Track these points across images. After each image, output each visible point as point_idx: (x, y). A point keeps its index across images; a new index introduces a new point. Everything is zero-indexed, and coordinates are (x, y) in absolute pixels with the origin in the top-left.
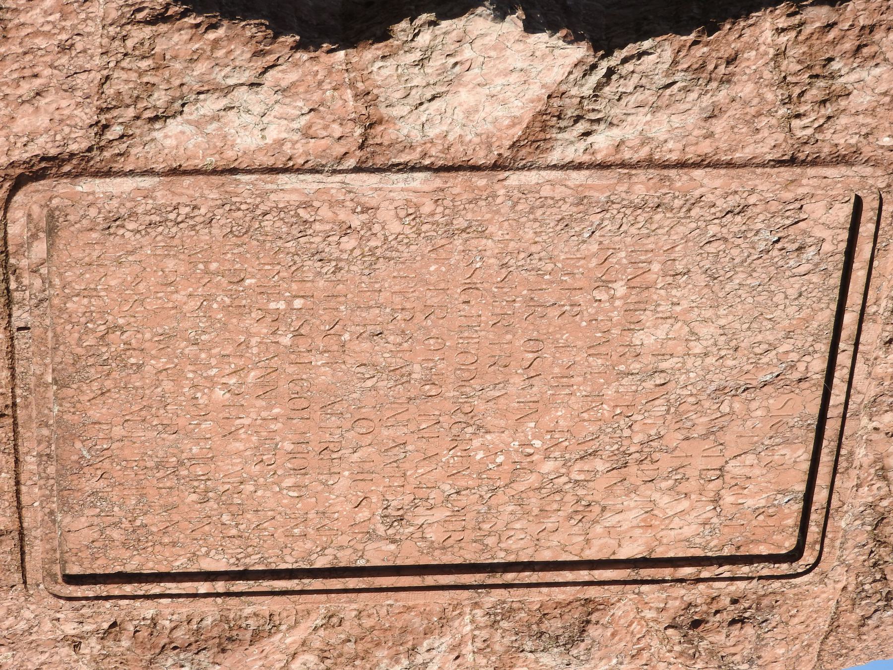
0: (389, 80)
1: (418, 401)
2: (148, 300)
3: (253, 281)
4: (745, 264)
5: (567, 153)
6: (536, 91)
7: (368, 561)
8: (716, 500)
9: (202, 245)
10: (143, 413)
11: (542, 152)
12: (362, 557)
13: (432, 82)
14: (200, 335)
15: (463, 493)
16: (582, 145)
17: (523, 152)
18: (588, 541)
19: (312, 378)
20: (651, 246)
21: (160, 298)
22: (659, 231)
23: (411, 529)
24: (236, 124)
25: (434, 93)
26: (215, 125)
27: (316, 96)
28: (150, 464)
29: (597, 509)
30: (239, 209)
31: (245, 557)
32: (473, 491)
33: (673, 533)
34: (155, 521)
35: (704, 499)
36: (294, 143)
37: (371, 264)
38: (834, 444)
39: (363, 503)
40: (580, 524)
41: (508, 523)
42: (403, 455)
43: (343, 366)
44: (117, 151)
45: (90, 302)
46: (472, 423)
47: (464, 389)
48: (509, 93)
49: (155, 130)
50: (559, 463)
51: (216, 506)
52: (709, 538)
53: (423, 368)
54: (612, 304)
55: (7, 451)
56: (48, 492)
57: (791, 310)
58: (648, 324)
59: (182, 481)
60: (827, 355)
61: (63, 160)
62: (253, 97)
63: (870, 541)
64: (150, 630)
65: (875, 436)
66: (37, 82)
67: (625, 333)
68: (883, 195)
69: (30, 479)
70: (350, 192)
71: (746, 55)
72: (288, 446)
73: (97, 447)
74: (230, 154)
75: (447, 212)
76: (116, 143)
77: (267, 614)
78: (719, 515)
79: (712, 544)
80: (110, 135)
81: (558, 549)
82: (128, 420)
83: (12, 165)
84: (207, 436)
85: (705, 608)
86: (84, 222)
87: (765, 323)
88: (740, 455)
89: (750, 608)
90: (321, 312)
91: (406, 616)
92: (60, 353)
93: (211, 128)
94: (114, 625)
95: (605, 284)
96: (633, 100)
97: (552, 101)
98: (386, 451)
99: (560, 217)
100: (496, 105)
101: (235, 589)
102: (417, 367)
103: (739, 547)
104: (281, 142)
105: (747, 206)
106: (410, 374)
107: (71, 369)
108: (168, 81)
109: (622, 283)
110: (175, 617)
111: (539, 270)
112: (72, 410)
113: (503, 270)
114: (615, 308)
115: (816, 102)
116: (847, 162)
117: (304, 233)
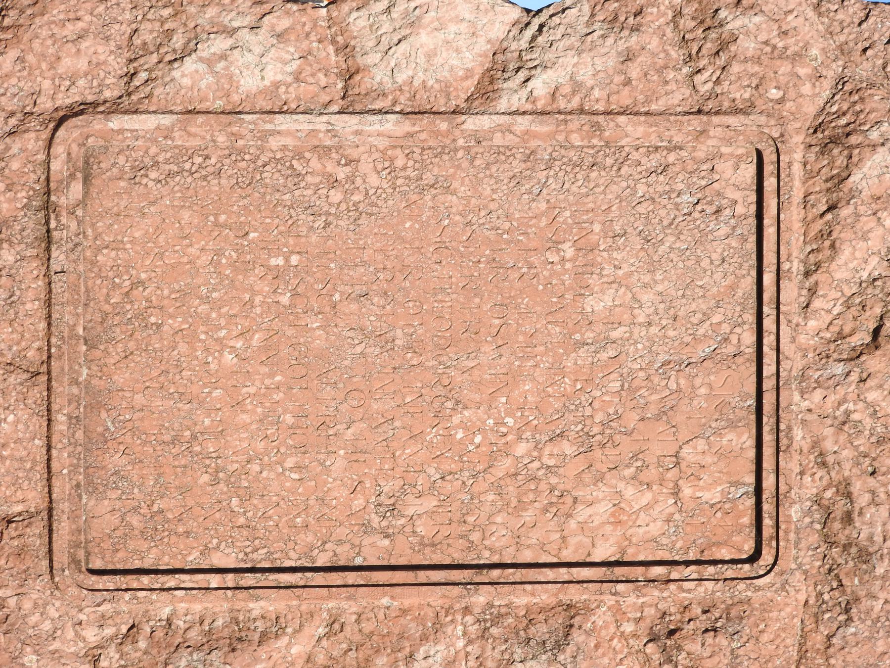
0: (363, 31)
1: (402, 371)
2: (167, 254)
3: (256, 235)
4: (673, 227)
5: (512, 102)
6: (482, 46)
7: (365, 559)
8: (676, 492)
9: (213, 195)
10: (161, 379)
11: (492, 101)
12: (359, 554)
13: (397, 27)
14: (211, 292)
15: (448, 478)
16: (524, 93)
17: (476, 103)
18: (564, 539)
19: (308, 342)
20: (591, 205)
21: (177, 252)
22: (597, 190)
23: (403, 521)
24: (240, 63)
25: (400, 37)
26: (223, 64)
27: (305, 45)
28: (167, 438)
29: (569, 500)
30: (244, 160)
31: (253, 552)
32: (456, 476)
33: (641, 531)
34: (169, 504)
35: (664, 491)
36: (288, 86)
37: (355, 220)
38: (773, 420)
39: (358, 489)
40: (555, 518)
41: (490, 516)
42: (391, 433)
43: (335, 330)
44: (143, 95)
45: (117, 255)
46: (450, 396)
47: (442, 359)
48: (460, 43)
49: (174, 69)
50: (531, 445)
51: (225, 489)
52: (674, 538)
53: (404, 334)
54: (563, 266)
55: (41, 414)
56: (75, 461)
57: (718, 276)
58: (596, 289)
59: (196, 459)
60: (755, 326)
61: (98, 104)
62: (253, 37)
63: (822, 544)
64: (165, 631)
65: (809, 417)
66: (80, 25)
67: (577, 298)
68: (779, 145)
69: (60, 441)
70: (335, 136)
71: (649, 10)
72: (289, 419)
73: (121, 418)
74: (236, 98)
75: (417, 165)
76: (142, 87)
77: (274, 617)
78: (680, 511)
79: (678, 545)
80: (136, 82)
81: (537, 547)
82: (148, 387)
83: (56, 110)
84: (218, 406)
85: (679, 617)
86: (115, 170)
87: (697, 290)
88: (691, 440)
89: (720, 618)
90: (314, 269)
91: (402, 621)
92: (90, 310)
93: (220, 66)
94: (133, 627)
95: (557, 243)
96: (561, 45)
97: (496, 57)
98: (376, 427)
99: (511, 174)
100: (450, 52)
101: (243, 583)
102: (399, 332)
103: (703, 552)
104: (276, 85)
105: (668, 166)
106: (393, 340)
107: (99, 329)
108: (185, 25)
109: (569, 244)
110: (188, 618)
111: (498, 228)
112: (99, 374)
113: (468, 228)
114: (566, 271)
115: (711, 55)
116: (744, 113)
117: (298, 186)
